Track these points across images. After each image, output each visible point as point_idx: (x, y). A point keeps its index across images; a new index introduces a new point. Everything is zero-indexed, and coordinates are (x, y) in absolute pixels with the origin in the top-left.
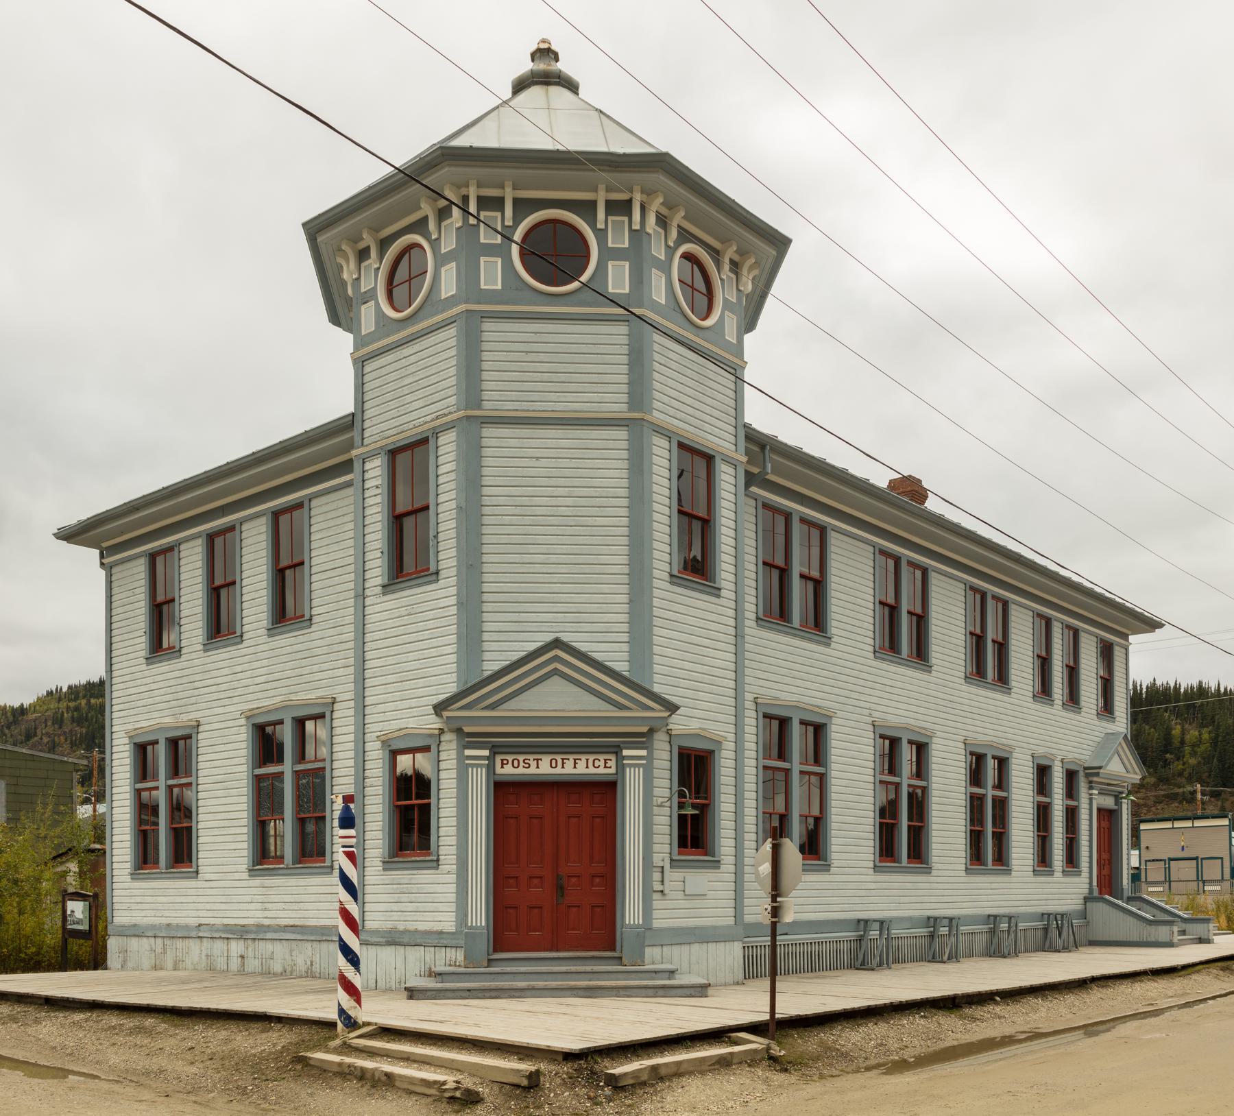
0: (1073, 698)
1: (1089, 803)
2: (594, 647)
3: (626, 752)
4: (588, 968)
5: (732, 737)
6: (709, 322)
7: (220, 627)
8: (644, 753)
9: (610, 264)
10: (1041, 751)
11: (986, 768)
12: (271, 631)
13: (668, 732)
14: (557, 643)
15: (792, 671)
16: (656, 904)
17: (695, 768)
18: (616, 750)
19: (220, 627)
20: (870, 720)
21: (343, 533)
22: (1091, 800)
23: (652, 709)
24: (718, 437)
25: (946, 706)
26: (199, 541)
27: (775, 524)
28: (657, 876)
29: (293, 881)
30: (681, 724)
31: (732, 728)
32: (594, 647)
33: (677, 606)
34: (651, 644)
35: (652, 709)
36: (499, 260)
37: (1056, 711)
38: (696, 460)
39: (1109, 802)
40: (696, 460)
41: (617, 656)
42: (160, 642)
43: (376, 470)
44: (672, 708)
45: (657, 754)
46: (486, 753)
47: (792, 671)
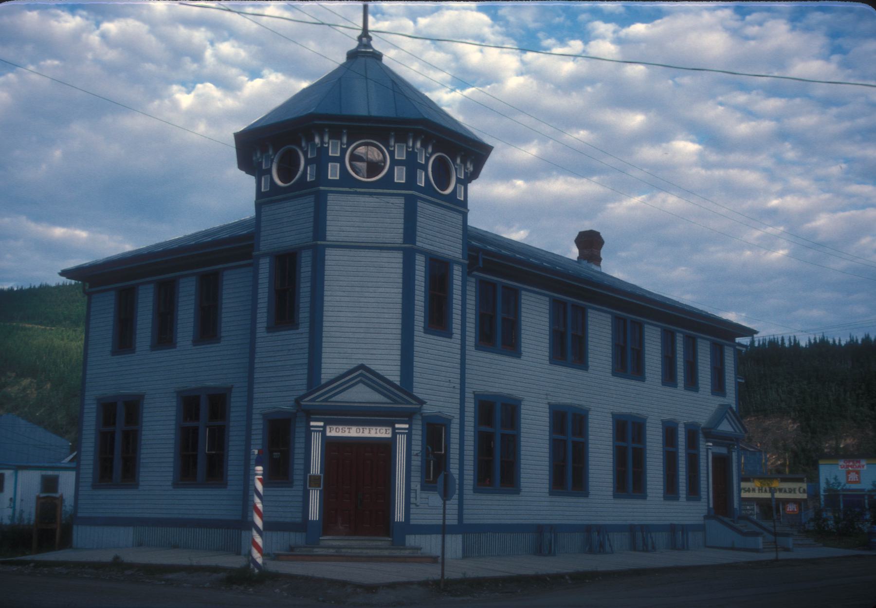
0: (692, 383)
1: (707, 450)
2: (382, 367)
3: (397, 426)
4: (365, 551)
5: (458, 416)
6: (449, 191)
7: (164, 337)
8: (407, 426)
9: (396, 168)
10: (667, 417)
11: (629, 430)
12: (196, 342)
13: (421, 414)
14: (362, 367)
15: (495, 374)
16: (412, 511)
17: (435, 432)
18: (391, 424)
19: (164, 337)
20: (546, 401)
21: (243, 295)
22: (707, 449)
23: (412, 404)
24: (452, 248)
25: (600, 392)
26: (152, 286)
27: (487, 295)
28: (413, 495)
29: (565, 571)
30: (429, 409)
31: (458, 411)
32: (382, 367)
33: (426, 344)
34: (412, 377)
35: (412, 404)
36: (338, 165)
37: (792, 335)
38: (439, 271)
39: (723, 451)
40: (439, 271)
41: (393, 373)
42: (124, 341)
43: (265, 267)
44: (422, 402)
45: (414, 427)
46: (322, 424)
47: (495, 374)
